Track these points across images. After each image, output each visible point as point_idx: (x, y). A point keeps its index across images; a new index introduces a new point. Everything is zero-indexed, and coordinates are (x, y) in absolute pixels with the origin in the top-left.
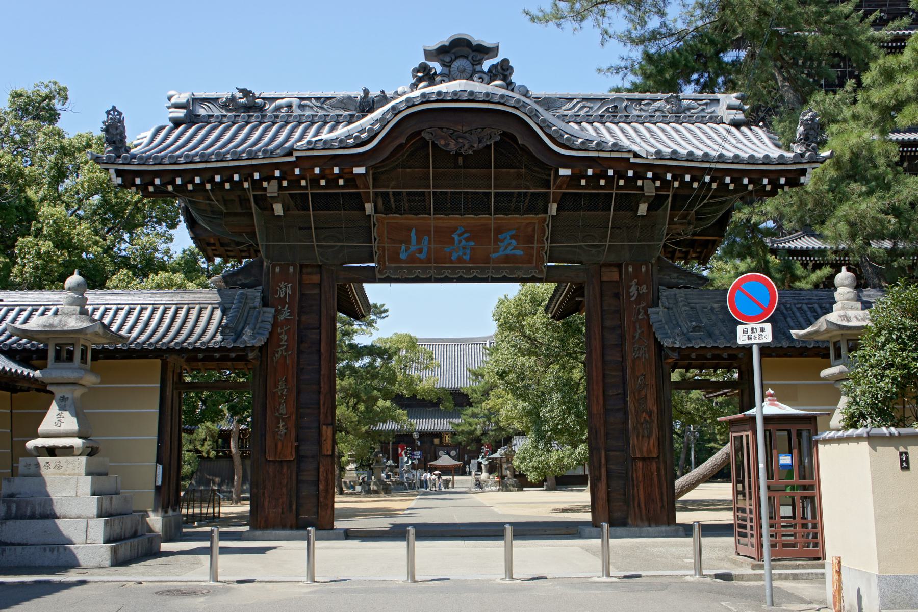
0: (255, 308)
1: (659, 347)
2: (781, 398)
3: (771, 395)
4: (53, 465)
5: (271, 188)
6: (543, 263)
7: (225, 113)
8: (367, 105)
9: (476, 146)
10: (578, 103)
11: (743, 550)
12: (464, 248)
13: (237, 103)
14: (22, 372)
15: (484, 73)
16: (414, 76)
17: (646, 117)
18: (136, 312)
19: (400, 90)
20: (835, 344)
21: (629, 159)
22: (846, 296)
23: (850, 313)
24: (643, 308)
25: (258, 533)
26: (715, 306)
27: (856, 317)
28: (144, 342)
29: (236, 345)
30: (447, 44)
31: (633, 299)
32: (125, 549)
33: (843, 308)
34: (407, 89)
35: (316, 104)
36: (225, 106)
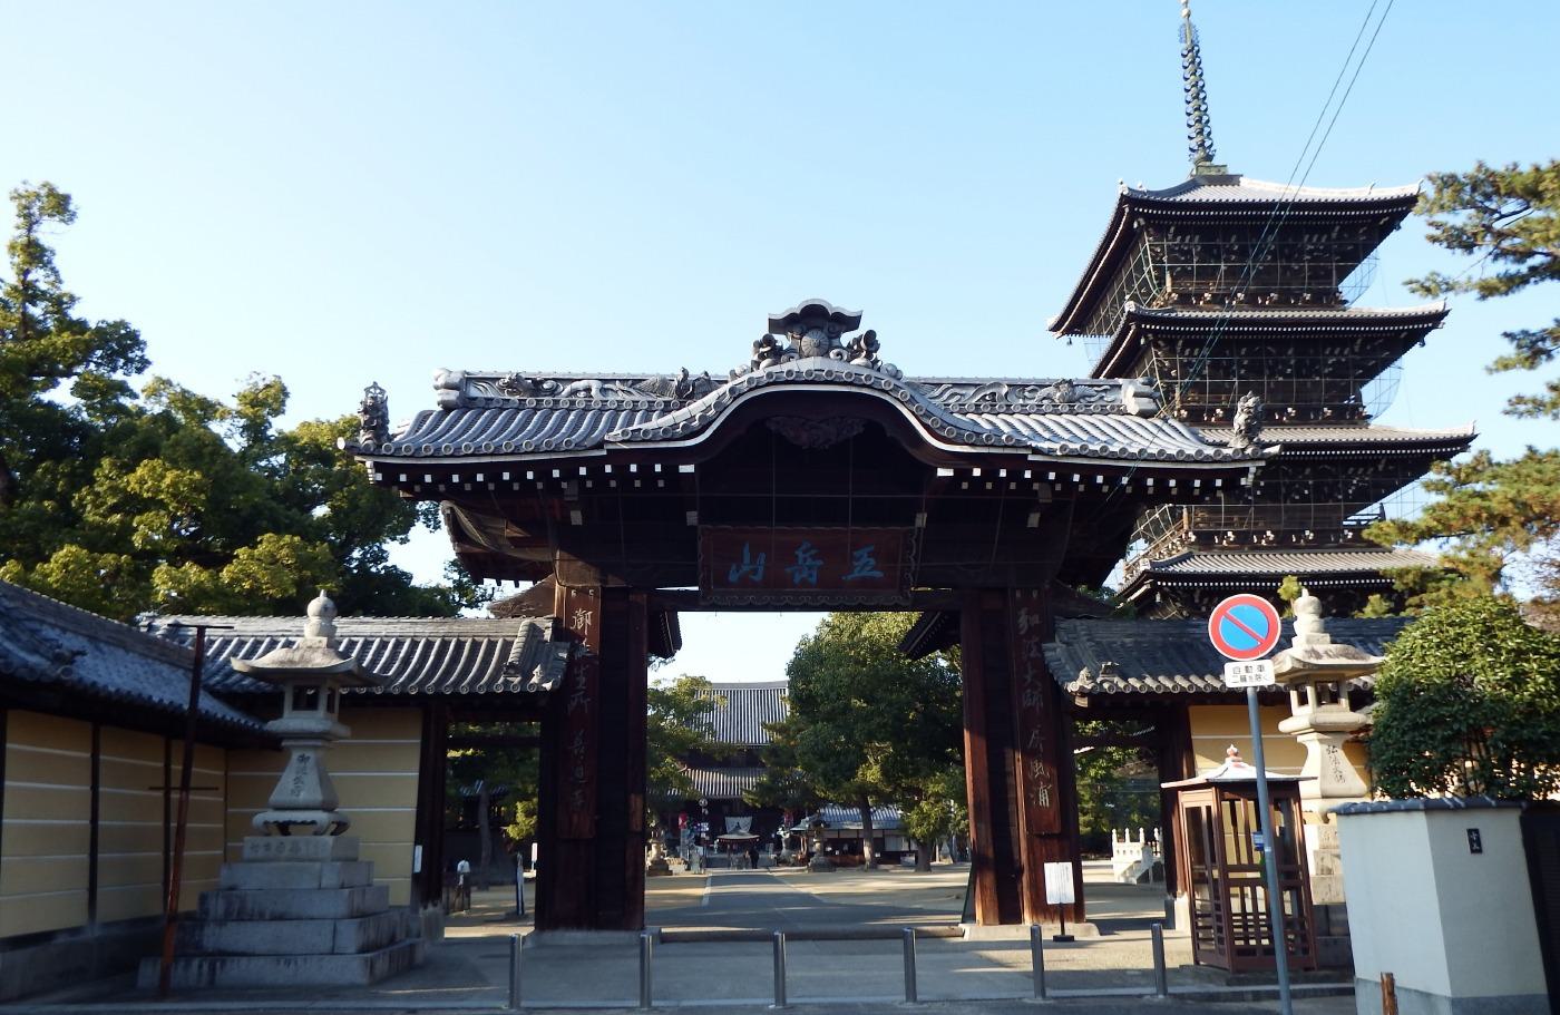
6: (909, 588)
8: (688, 389)
10: (948, 388)
14: (239, 720)
21: (1026, 456)
23: (1320, 648)
24: (1036, 644)
26: (1128, 640)
27: (1326, 653)
31: (1022, 633)
35: (622, 388)
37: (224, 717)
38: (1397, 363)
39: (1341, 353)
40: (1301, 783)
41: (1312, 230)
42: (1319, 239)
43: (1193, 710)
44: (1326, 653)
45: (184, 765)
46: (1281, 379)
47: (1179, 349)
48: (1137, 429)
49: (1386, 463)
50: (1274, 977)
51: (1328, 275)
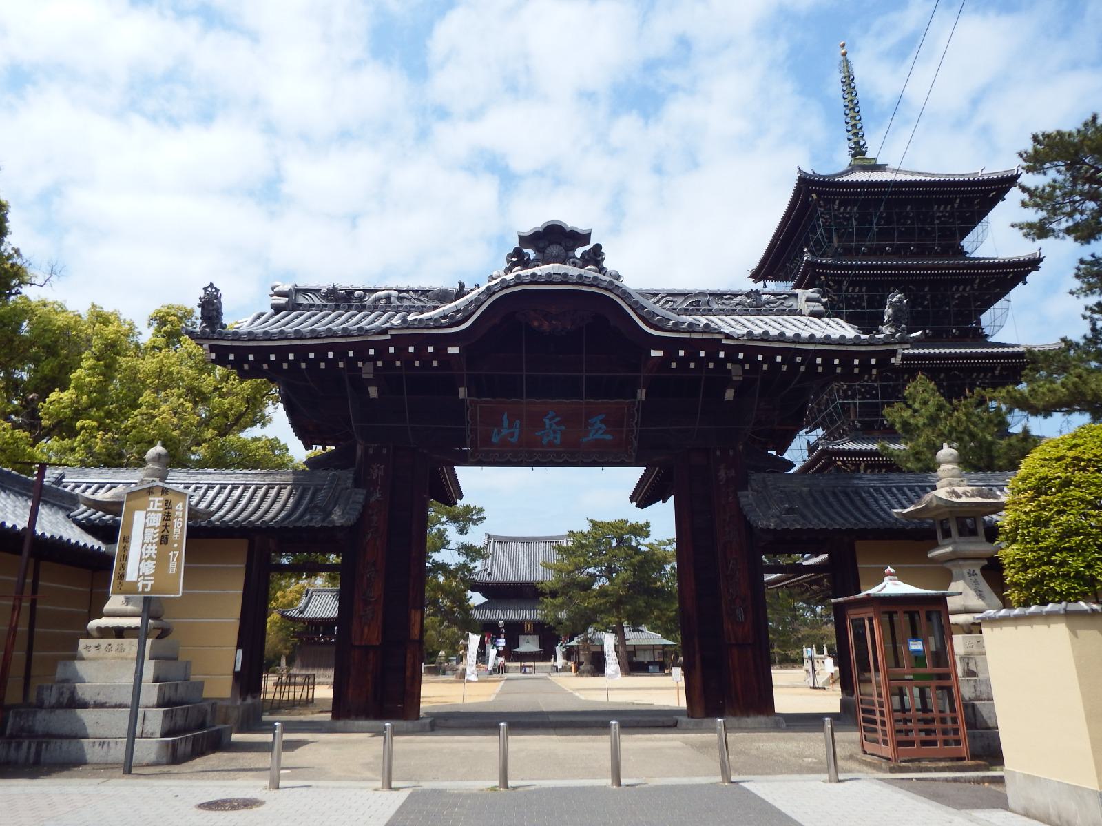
0: (347, 488)
1: (749, 527)
2: (903, 577)
3: (891, 574)
4: (115, 647)
5: (366, 370)
7: (325, 302)
9: (569, 327)
10: (663, 297)
11: (869, 747)
12: (555, 432)
13: (338, 294)
14: (99, 548)
16: (508, 261)
17: (728, 310)
19: (495, 274)
23: (959, 490)
25: (340, 723)
28: (231, 520)
29: (324, 524)
30: (541, 230)
34: (502, 273)
36: (325, 297)
37: (93, 547)
38: (1006, 297)
39: (964, 290)
40: (949, 599)
41: (939, 202)
42: (945, 208)
43: (859, 545)
44: (964, 493)
46: (920, 309)
49: (1001, 370)
50: (981, 650)
51: (953, 234)
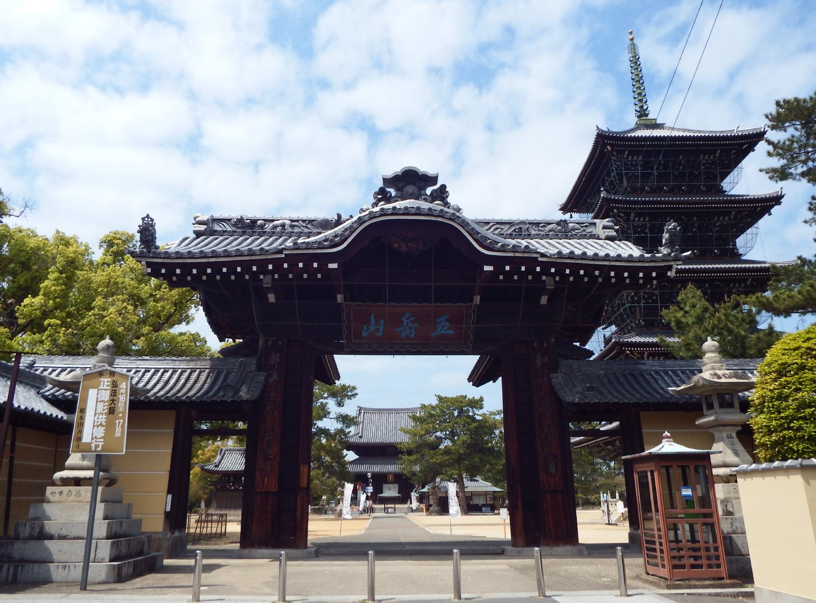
0: (252, 372)
1: (559, 401)
2: (677, 439)
4: (74, 493)
5: (266, 281)
10: (494, 225)
12: (410, 328)
13: (244, 223)
14: (62, 417)
15: (427, 195)
16: (375, 198)
17: (543, 235)
18: (160, 373)
19: (365, 207)
20: (706, 397)
21: (537, 258)
22: (713, 360)
23: (720, 373)
32: (127, 566)
33: (713, 368)
34: (370, 207)
36: (235, 225)
38: (756, 225)
43: (643, 414)
44: (724, 375)
45: (15, 445)
46: (690, 234)
47: (632, 218)
48: (605, 245)
